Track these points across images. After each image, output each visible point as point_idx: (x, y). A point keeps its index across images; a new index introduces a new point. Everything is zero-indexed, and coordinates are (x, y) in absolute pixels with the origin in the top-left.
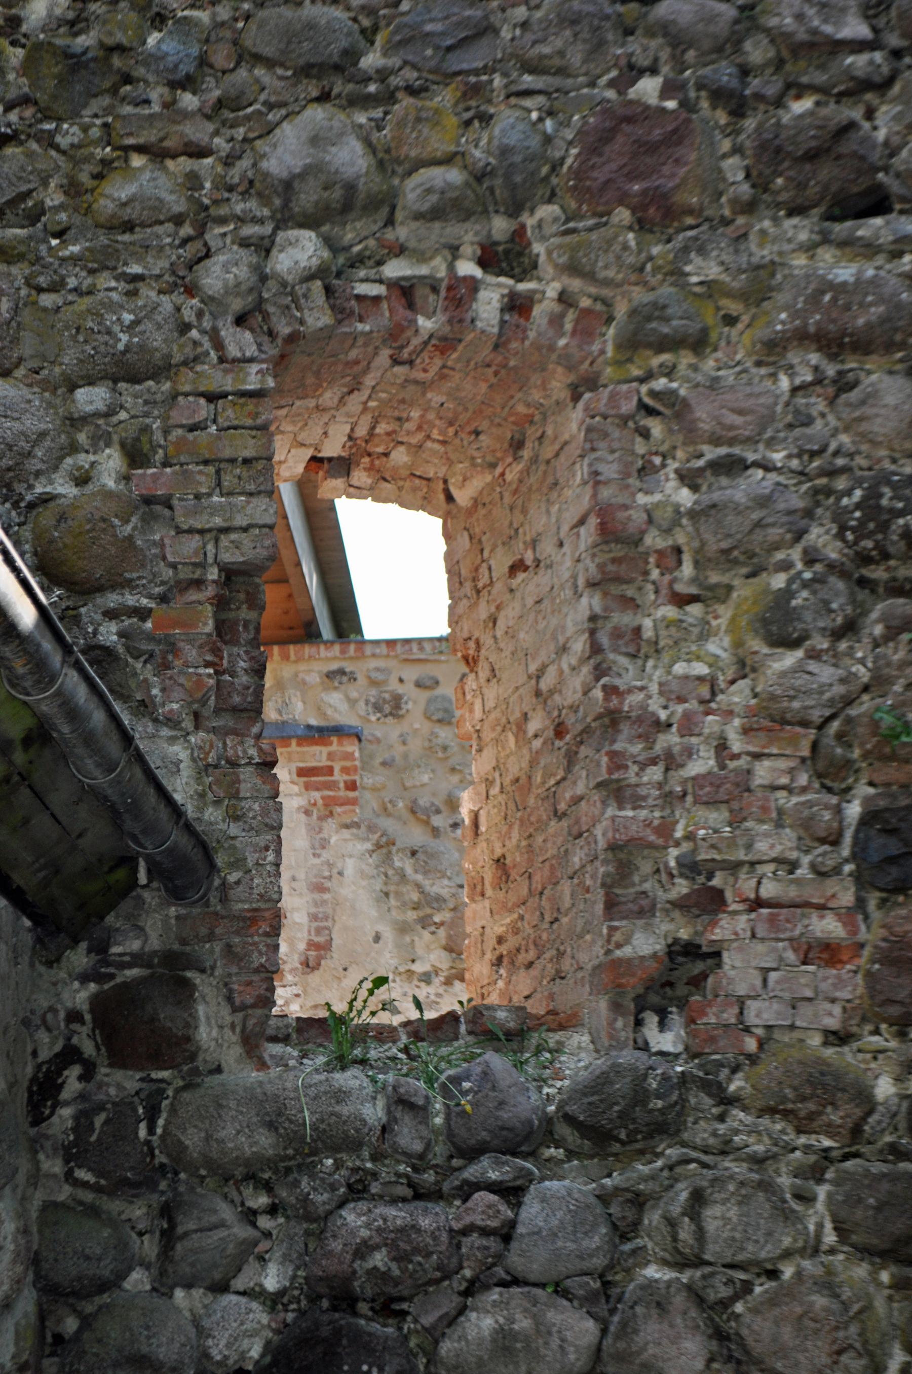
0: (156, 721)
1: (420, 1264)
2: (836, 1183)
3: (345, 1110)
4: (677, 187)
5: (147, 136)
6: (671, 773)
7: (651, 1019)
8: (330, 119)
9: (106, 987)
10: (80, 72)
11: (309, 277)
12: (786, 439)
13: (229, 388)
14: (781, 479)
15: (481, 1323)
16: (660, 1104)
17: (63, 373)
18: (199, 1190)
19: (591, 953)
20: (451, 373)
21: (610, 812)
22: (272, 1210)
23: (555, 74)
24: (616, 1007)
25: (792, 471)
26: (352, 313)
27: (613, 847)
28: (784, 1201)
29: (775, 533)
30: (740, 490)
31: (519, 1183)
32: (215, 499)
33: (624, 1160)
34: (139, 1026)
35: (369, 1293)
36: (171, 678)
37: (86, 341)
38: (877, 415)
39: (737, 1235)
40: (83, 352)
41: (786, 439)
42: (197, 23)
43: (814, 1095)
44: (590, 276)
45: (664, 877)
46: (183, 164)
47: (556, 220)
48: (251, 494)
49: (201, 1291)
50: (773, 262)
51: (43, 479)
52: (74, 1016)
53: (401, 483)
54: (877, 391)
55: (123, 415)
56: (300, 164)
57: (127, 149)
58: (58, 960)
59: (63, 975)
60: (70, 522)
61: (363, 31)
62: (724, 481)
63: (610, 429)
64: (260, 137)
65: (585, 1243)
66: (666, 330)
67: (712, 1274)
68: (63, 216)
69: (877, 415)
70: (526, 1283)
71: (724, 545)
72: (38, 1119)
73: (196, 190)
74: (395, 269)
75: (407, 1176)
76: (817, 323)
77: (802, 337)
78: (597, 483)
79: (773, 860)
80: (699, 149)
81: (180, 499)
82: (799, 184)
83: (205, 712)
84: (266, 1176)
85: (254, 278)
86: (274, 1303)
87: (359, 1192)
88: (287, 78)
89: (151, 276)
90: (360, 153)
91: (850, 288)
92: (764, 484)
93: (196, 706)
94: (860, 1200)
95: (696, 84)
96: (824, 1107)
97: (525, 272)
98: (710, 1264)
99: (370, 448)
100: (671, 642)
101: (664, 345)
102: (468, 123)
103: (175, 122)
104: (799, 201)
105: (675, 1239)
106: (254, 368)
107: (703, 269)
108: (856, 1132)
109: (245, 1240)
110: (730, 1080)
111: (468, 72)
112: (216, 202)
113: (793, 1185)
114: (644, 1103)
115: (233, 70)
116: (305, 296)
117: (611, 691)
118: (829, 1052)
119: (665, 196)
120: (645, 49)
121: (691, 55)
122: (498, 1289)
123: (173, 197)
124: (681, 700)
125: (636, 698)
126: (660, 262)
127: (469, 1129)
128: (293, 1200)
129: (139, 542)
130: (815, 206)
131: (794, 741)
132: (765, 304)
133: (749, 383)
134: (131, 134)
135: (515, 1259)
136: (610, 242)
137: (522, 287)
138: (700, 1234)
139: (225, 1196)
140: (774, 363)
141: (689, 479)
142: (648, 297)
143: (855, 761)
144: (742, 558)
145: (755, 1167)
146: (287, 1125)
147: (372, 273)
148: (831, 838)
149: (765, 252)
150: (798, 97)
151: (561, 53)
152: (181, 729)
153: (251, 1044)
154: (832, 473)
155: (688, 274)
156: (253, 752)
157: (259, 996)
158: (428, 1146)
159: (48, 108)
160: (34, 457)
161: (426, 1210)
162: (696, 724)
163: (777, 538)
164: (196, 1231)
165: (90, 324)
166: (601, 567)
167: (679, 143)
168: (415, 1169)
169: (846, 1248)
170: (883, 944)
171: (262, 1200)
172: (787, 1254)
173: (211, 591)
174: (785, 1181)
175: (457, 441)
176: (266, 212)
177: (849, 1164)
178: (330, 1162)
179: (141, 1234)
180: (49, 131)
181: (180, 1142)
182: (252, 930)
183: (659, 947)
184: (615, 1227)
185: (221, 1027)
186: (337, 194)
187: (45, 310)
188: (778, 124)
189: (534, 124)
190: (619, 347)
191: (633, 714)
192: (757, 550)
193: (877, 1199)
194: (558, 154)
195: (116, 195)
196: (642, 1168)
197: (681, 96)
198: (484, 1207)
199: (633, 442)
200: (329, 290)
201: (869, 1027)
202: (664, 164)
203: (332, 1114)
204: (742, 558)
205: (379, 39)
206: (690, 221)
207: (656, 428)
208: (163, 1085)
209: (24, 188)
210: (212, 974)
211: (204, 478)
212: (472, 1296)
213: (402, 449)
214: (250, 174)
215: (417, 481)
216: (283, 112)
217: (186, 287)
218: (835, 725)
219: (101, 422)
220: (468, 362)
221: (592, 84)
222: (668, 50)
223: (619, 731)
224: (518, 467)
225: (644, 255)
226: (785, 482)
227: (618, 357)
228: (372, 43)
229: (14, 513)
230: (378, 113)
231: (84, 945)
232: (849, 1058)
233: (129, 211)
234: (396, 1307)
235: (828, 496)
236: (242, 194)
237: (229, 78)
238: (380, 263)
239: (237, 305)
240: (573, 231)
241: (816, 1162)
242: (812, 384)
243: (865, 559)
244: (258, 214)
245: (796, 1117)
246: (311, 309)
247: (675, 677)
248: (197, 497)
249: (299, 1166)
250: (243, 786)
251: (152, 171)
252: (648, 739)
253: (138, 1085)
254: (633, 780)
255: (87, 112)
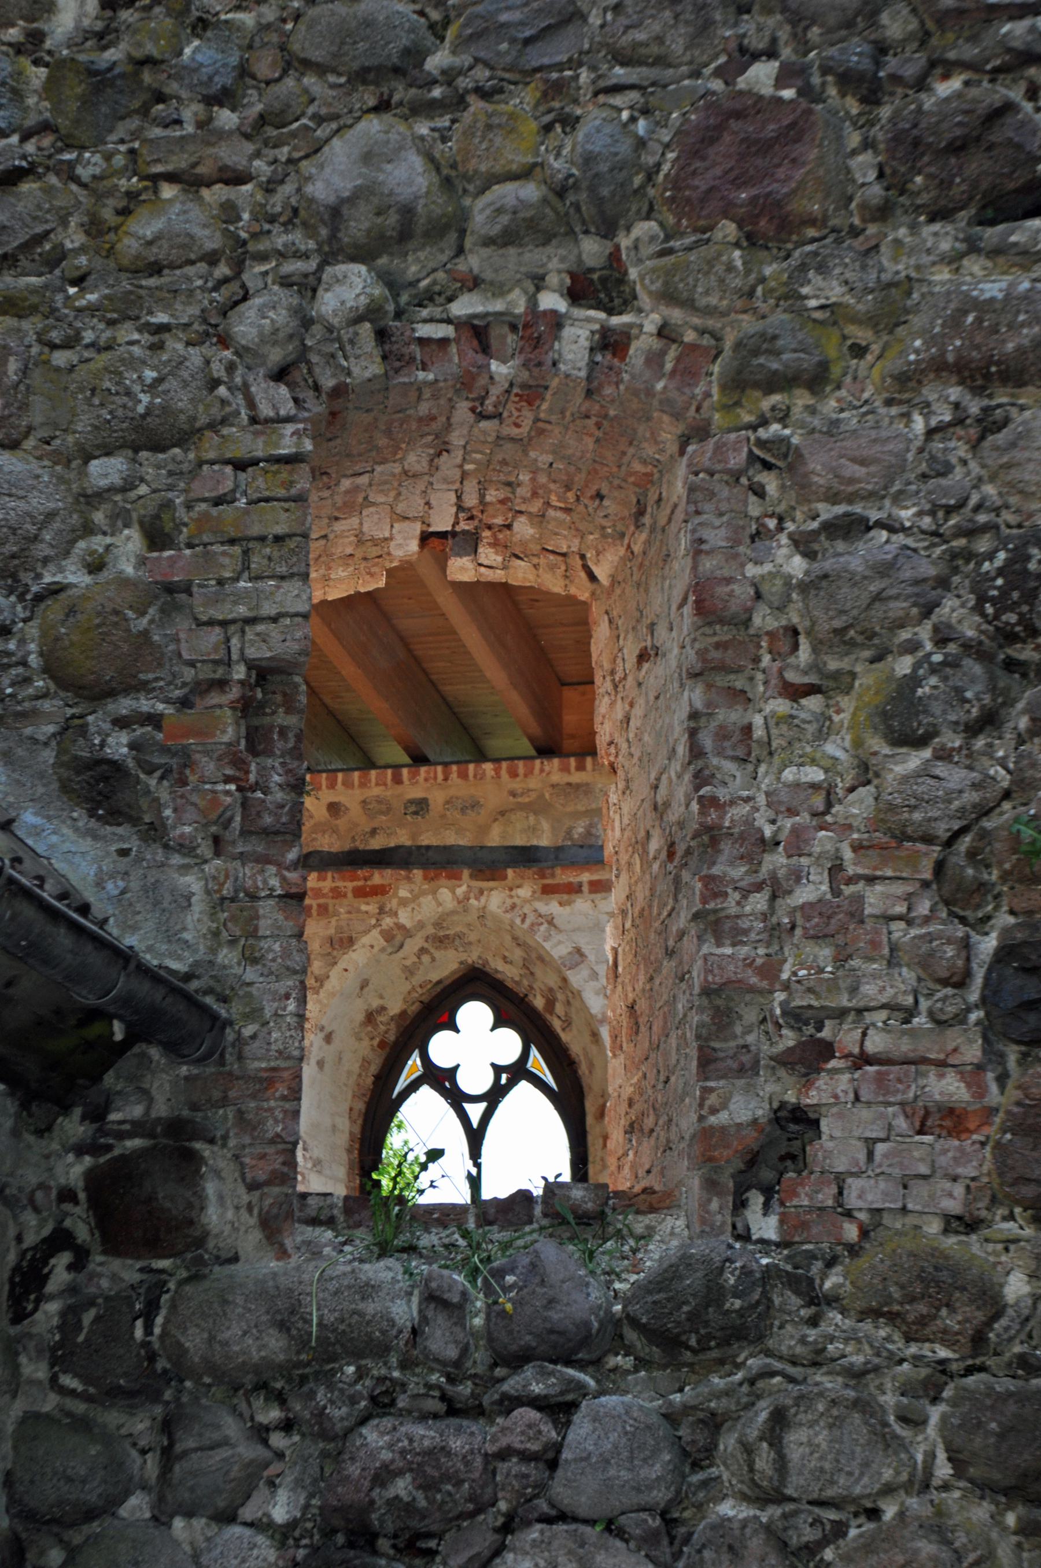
0: (166, 846)
1: (450, 1494)
2: (954, 1403)
3: (370, 1308)
4: (794, 192)
5: (178, 162)
6: (779, 901)
7: (756, 1199)
8: (387, 132)
9: (102, 1160)
10: (109, 91)
11: (358, 320)
12: (917, 492)
13: (260, 454)
14: (910, 542)
16: (738, 1303)
17: (77, 443)
18: (204, 1401)
20: (548, 427)
21: (705, 949)
22: (287, 1426)
23: (653, 65)
24: (711, 1185)
25: (923, 532)
26: (413, 359)
27: (707, 992)
28: (886, 1424)
29: (897, 608)
30: (856, 557)
31: (570, 1397)
32: (242, 584)
33: (700, 1371)
34: (137, 1206)
35: (390, 1527)
36: (182, 797)
37: (102, 405)
38: (1030, 460)
39: (827, 1466)
40: (99, 416)
41: (917, 492)
42: (239, 27)
43: (928, 1293)
44: (689, 304)
45: (770, 1027)
46: (215, 194)
47: (653, 239)
48: (282, 578)
49: (204, 1520)
50: (909, 278)
51: (52, 567)
52: (67, 1195)
53: (535, 560)
54: (1029, 431)
55: (143, 489)
56: (350, 186)
57: (155, 179)
58: (49, 1128)
59: (55, 1146)
60: (79, 616)
61: (432, 26)
62: (840, 546)
63: (717, 487)
64: (307, 156)
65: (644, 1472)
66: (775, 366)
67: (795, 1513)
68: (83, 260)
69: (1030, 460)
70: (575, 1519)
71: (837, 624)
72: (19, 1316)
73: (232, 223)
74: (464, 306)
75: (438, 1387)
76: (958, 350)
78: (698, 553)
79: (883, 1007)
80: (820, 146)
81: (200, 586)
82: (942, 182)
83: (228, 836)
84: (278, 1385)
85: (294, 323)
86: (285, 1537)
87: (385, 1406)
88: (341, 86)
89: (178, 326)
90: (420, 170)
91: (998, 306)
92: (887, 547)
93: (213, 829)
94: (979, 1424)
95: (820, 67)
96: (938, 1309)
97: (625, 303)
98: (791, 1499)
99: (486, 519)
100: (784, 744)
101: (773, 383)
102: (548, 128)
103: (209, 144)
104: (943, 202)
105: (751, 1470)
106: (289, 428)
107: (822, 291)
108: (979, 1340)
109: (252, 1461)
110: (824, 1277)
111: (550, 68)
112: (254, 236)
113: (898, 1405)
114: (719, 1302)
115: (278, 80)
116: (352, 342)
117: (709, 803)
118: (952, 1240)
119: (778, 204)
120: (760, 29)
121: (815, 33)
122: (539, 1526)
123: (207, 232)
124: (792, 812)
125: (742, 810)
126: (773, 284)
127: (510, 1332)
128: (307, 1415)
129: (156, 638)
130: (962, 209)
131: (913, 861)
132: (900, 329)
133: (877, 426)
134: (158, 161)
135: (560, 1489)
136: (710, 263)
137: (615, 320)
138: (781, 1464)
139: (234, 1409)
140: (908, 401)
141: (803, 545)
142: (758, 326)
143: (993, 885)
144: (860, 639)
145: (852, 1383)
146: (300, 1325)
147: (437, 312)
148: (955, 979)
149: (900, 267)
150: (946, 77)
151: (659, 39)
152: (196, 856)
153: (270, 1229)
154: (972, 532)
155: (806, 297)
156: (274, 882)
157: (273, 1172)
158: (465, 1351)
159: (70, 136)
160: (42, 541)
161: (459, 1430)
162: (807, 842)
163: (901, 613)
164: (196, 1450)
165: (107, 384)
166: (702, 654)
167: (797, 140)
168: (451, 1380)
169: (962, 1484)
170: (1016, 1109)
171: (274, 1414)
172: (888, 1490)
173: (235, 693)
174: (889, 1399)
175: (581, 508)
176: (312, 245)
177: (970, 1380)
178: (351, 1369)
179: (143, 1452)
180: (69, 162)
181: (179, 1345)
182: (269, 1093)
183: (763, 1112)
184: (685, 1454)
185: (237, 1208)
186: (393, 219)
187: (58, 369)
188: (919, 110)
189: (625, 125)
190: (723, 388)
191: (736, 830)
192: (877, 629)
193: (1000, 1423)
194: (651, 160)
195: (141, 232)
196: (717, 1381)
197: (800, 83)
198: (525, 1426)
199: (746, 503)
200: (382, 335)
201: (1001, 1212)
202: (779, 165)
203: (355, 1312)
204: (860, 639)
205: (450, 33)
206: (812, 232)
207: (771, 483)
208: (164, 1277)
209: (39, 229)
210: (224, 1145)
211: (228, 559)
212: (512, 1532)
213: (523, 519)
214: (293, 201)
215: (551, 557)
216: (334, 126)
217: (219, 336)
218: (967, 840)
219: (118, 498)
220: (562, 412)
221: (696, 74)
222: (788, 28)
223: (719, 851)
224: (643, 536)
225: (753, 276)
226: (913, 545)
227: (725, 400)
228: (442, 39)
229: (19, 608)
230: (444, 122)
231: (78, 1111)
232: (976, 1249)
233: (155, 250)
234: (423, 1544)
235: (968, 561)
236: (284, 224)
237: (275, 88)
238: (450, 300)
239: (276, 356)
240: (670, 251)
241: (928, 1377)
242: (951, 424)
243: (1009, 637)
244: (303, 247)
245: (904, 1320)
246: (357, 357)
247: (785, 785)
248: (221, 582)
249: (317, 1373)
250: (262, 923)
251: (183, 203)
252: (751, 859)
253: (137, 1277)
254: (733, 910)
255: (113, 137)
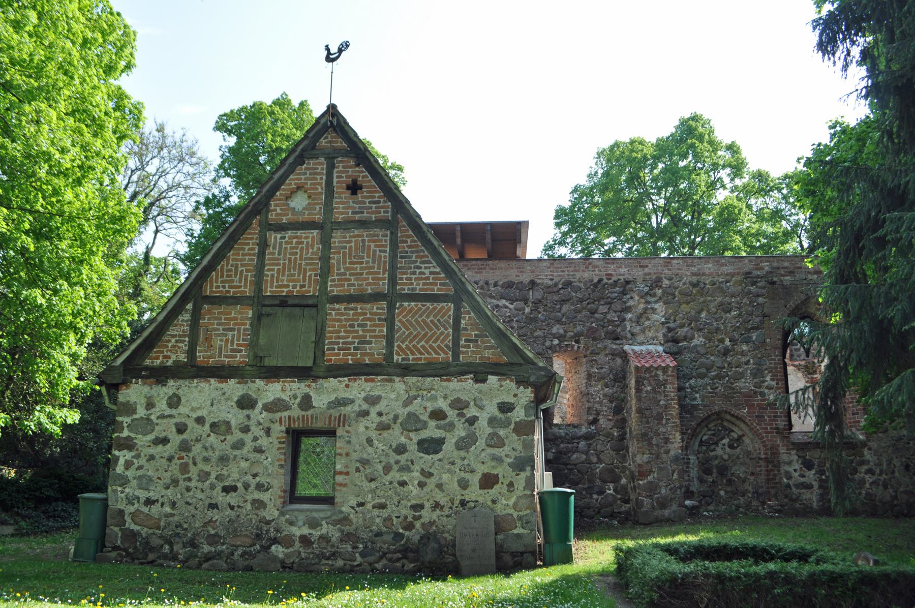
15: (575, 456)
19: (585, 418)
30: (603, 371)
107: (599, 345)
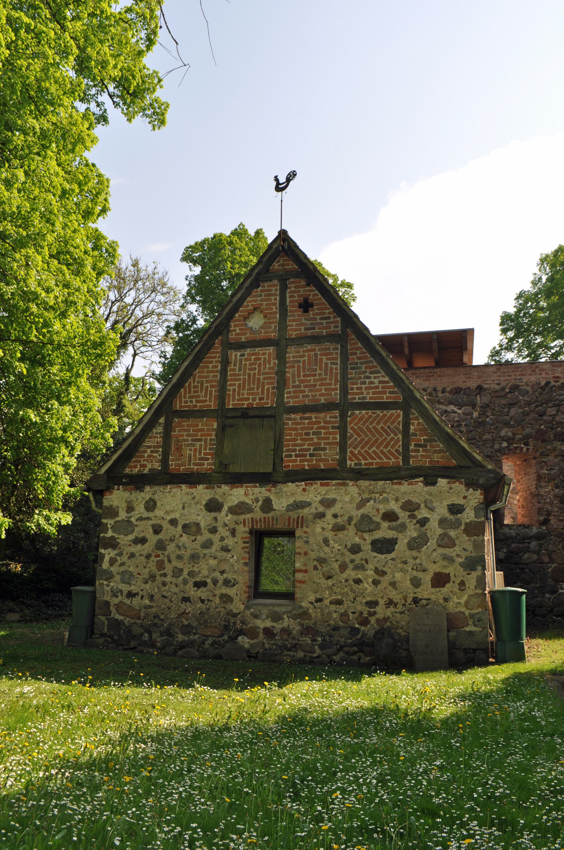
15: (526, 556)
74: (515, 445)
77: (559, 455)
107: (548, 447)
198: (526, 545)
